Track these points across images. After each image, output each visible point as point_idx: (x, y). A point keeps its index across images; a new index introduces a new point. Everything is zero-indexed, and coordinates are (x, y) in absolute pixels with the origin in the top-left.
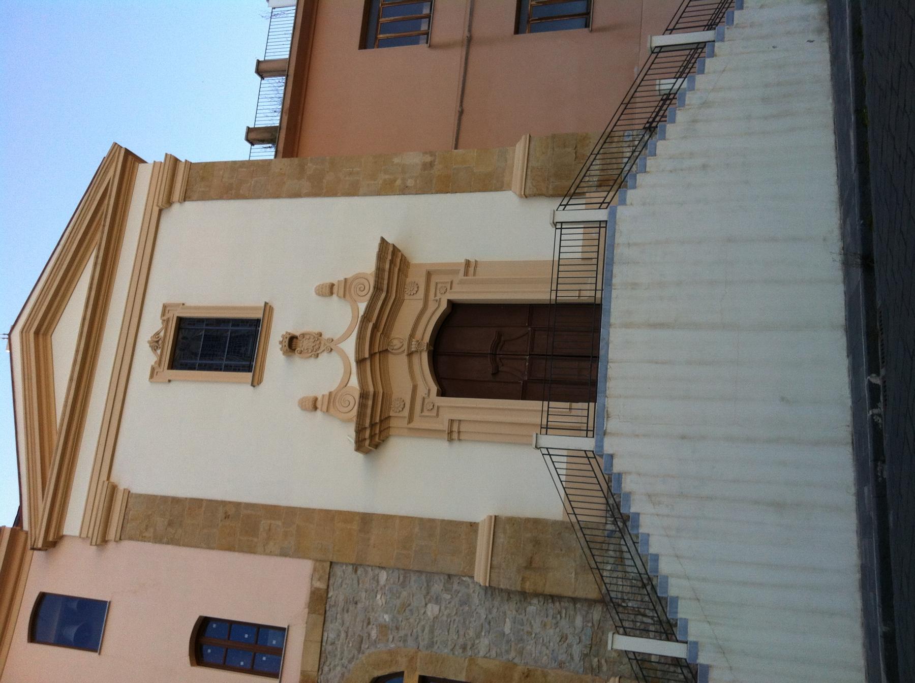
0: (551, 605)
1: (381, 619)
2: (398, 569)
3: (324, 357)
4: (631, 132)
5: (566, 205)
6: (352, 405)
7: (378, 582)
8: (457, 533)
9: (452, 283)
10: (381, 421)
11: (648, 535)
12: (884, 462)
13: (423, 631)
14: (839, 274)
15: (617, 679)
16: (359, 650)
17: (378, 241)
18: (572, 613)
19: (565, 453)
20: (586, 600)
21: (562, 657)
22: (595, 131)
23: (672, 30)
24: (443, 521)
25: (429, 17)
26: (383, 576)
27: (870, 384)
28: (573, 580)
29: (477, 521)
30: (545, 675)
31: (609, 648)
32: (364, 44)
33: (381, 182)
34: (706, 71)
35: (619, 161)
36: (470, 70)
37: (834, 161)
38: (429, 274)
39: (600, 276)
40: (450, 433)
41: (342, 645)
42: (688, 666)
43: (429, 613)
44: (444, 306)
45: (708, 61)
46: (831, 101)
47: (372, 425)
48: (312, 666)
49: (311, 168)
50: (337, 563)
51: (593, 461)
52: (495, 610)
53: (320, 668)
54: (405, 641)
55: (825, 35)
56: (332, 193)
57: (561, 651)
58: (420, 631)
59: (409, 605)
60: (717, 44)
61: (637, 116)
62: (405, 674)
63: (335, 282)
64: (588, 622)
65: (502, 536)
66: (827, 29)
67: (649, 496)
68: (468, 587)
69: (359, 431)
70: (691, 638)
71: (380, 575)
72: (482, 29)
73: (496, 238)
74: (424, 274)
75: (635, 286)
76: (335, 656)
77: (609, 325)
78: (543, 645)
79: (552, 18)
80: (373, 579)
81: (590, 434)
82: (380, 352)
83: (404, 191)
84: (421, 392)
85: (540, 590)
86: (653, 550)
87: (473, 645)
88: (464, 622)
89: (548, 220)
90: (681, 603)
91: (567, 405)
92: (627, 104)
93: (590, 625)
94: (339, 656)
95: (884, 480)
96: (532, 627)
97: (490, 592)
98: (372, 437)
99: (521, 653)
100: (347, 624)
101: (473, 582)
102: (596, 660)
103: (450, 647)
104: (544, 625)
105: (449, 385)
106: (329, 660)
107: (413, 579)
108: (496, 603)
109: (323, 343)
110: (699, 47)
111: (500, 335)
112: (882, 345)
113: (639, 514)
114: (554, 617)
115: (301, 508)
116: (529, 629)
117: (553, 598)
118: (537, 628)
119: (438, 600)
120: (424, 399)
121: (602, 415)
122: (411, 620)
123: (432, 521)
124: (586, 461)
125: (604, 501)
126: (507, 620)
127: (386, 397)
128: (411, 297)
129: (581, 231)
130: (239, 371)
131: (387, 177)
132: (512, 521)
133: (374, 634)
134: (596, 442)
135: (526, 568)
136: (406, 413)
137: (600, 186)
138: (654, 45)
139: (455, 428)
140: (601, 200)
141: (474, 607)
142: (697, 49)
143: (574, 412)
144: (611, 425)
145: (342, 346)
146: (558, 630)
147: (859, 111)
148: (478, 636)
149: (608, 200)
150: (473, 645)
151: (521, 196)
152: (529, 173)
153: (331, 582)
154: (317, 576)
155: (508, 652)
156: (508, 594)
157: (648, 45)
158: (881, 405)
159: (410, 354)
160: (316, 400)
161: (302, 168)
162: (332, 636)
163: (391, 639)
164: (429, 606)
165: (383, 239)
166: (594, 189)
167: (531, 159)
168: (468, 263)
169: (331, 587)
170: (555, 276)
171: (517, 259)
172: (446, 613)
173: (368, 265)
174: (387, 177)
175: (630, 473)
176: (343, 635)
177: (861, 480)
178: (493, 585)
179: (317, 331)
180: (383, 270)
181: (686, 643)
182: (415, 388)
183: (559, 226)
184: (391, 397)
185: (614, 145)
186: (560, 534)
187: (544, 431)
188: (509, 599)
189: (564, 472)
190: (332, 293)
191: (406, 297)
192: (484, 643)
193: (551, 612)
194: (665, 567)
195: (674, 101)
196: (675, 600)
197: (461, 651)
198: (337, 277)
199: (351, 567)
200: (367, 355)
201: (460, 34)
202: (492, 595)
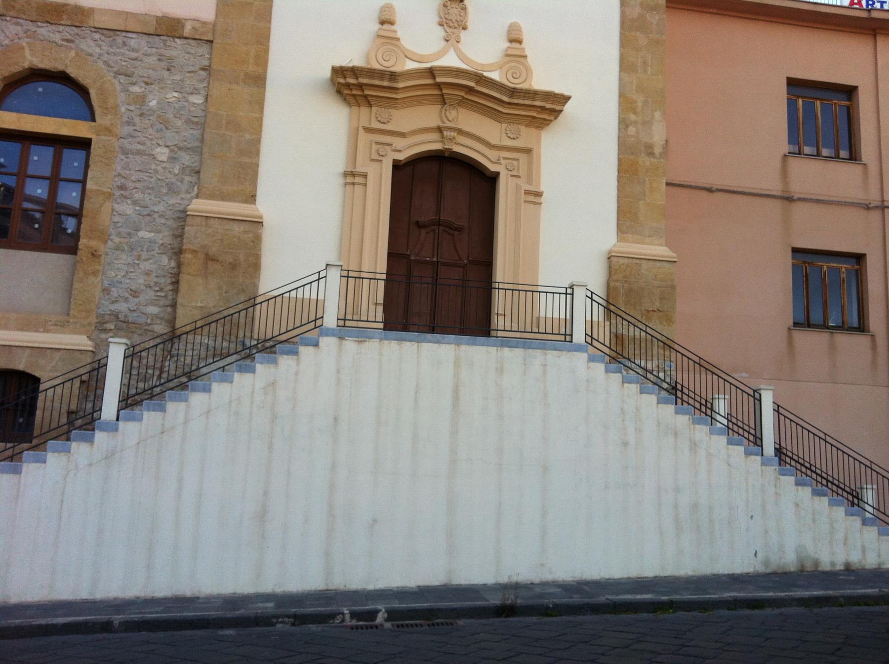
0: (169, 281)
1: (151, 97)
2: (205, 116)
3: (440, 32)
4: (673, 368)
5: (591, 298)
6: (385, 64)
7: (192, 94)
8: (244, 181)
9: (519, 177)
10: (366, 96)
11: (232, 382)
12: (293, 624)
13: (139, 143)
14: (504, 579)
15: (91, 349)
16: (118, 73)
17: (566, 93)
18: (161, 303)
19: (321, 297)
20: (175, 318)
21: (114, 292)
22: (676, 333)
23: (778, 411)
24: (257, 165)
25: (819, 154)
26: (198, 99)
27: (377, 612)
28: (194, 304)
29: (257, 203)
30: (95, 273)
31: (110, 340)
32: (793, 83)
33: (634, 97)
34: (731, 447)
35: (643, 357)
36: (756, 200)
37: (626, 576)
38: (528, 151)
39: (518, 335)
40: (353, 174)
41: (124, 54)
42: (93, 420)
43: (158, 150)
44: (493, 168)
45: (741, 449)
46: (690, 573)
47: (361, 86)
48: (99, 21)
49: (654, 19)
50: (211, 48)
51: (312, 325)
52: (163, 221)
53: (98, 29)
54: (128, 123)
55: (761, 569)
56: (625, 42)
57: (120, 291)
58: (138, 140)
59: (167, 128)
60: (759, 458)
61: (691, 375)
62: (93, 124)
63: (523, 45)
64: (152, 319)
65: (242, 229)
66: (768, 571)
67: (273, 384)
68: (188, 192)
69: (354, 71)
70: (121, 423)
71: (198, 96)
72: (800, 211)
73: (565, 226)
74: (530, 146)
75: (500, 370)
76: (111, 46)
77: (458, 344)
78: (127, 272)
79: (807, 288)
80: (195, 89)
81: (341, 323)
82: (442, 95)
83: (623, 124)
84: (399, 143)
85: (184, 269)
86: (215, 386)
87: (126, 197)
88: (149, 188)
89: (575, 279)
90: (159, 414)
91: (381, 299)
92: (703, 365)
93: (149, 321)
94: (111, 50)
95: (274, 625)
96: (146, 260)
97: (182, 215)
98: (348, 86)
99: (118, 248)
100: (146, 59)
101: (192, 198)
102: (112, 327)
103: (122, 172)
104: (148, 273)
105: (410, 176)
106: (107, 40)
107: (195, 132)
108: (169, 223)
109: (455, 31)
110: (758, 440)
111: (460, 229)
112: (416, 625)
113: (254, 372)
114: (156, 283)
115: (271, 6)
116: (143, 257)
117: (176, 283)
118: (145, 266)
119: (173, 159)
120: (391, 145)
121: (362, 334)
122: (150, 130)
123: (258, 153)
124: (312, 318)
125: (269, 336)
126: (153, 234)
127: (392, 103)
128: (503, 131)
129: (563, 316)
131: (640, 104)
132: (257, 240)
133: (136, 89)
134: (333, 329)
135: (207, 255)
136: (375, 125)
137: (616, 336)
138: (763, 393)
139: (357, 180)
140: (595, 336)
141: (165, 198)
142: (755, 436)
143: (372, 307)
144: (350, 345)
145: (452, 53)
146: (143, 287)
147: (672, 605)
148: (135, 203)
149: (595, 343)
150: (126, 197)
151: (610, 252)
152: (635, 261)
153: (191, 41)
154: (197, 25)
155: (119, 234)
156: (180, 236)
157: (762, 387)
158: (354, 622)
159: (439, 130)
160: (392, 23)
161: (653, 9)
162: (133, 43)
163: (132, 108)
164: (166, 150)
165: (568, 98)
166: (613, 330)
167: (651, 263)
168: (539, 194)
169: (185, 41)
170: (520, 287)
171: (541, 249)
172: (159, 168)
173: (540, 82)
174: (640, 104)
175: (298, 364)
176: (134, 55)
177: (285, 600)
178: (189, 219)
179: (470, 24)
180: (534, 99)
181: (118, 420)
182: (402, 135)
183: (569, 291)
184: (392, 108)
185: (661, 351)
186: (243, 291)
187: (345, 273)
188: (175, 236)
189: (300, 296)
190: (511, 41)
191: (504, 126)
192: (128, 209)
193: (162, 280)
194: (197, 399)
195: (697, 412)
196: (163, 409)
197: (119, 184)
198: (528, 47)
199: (207, 63)
200: (439, 80)
201: (797, 188)
202: (179, 218)
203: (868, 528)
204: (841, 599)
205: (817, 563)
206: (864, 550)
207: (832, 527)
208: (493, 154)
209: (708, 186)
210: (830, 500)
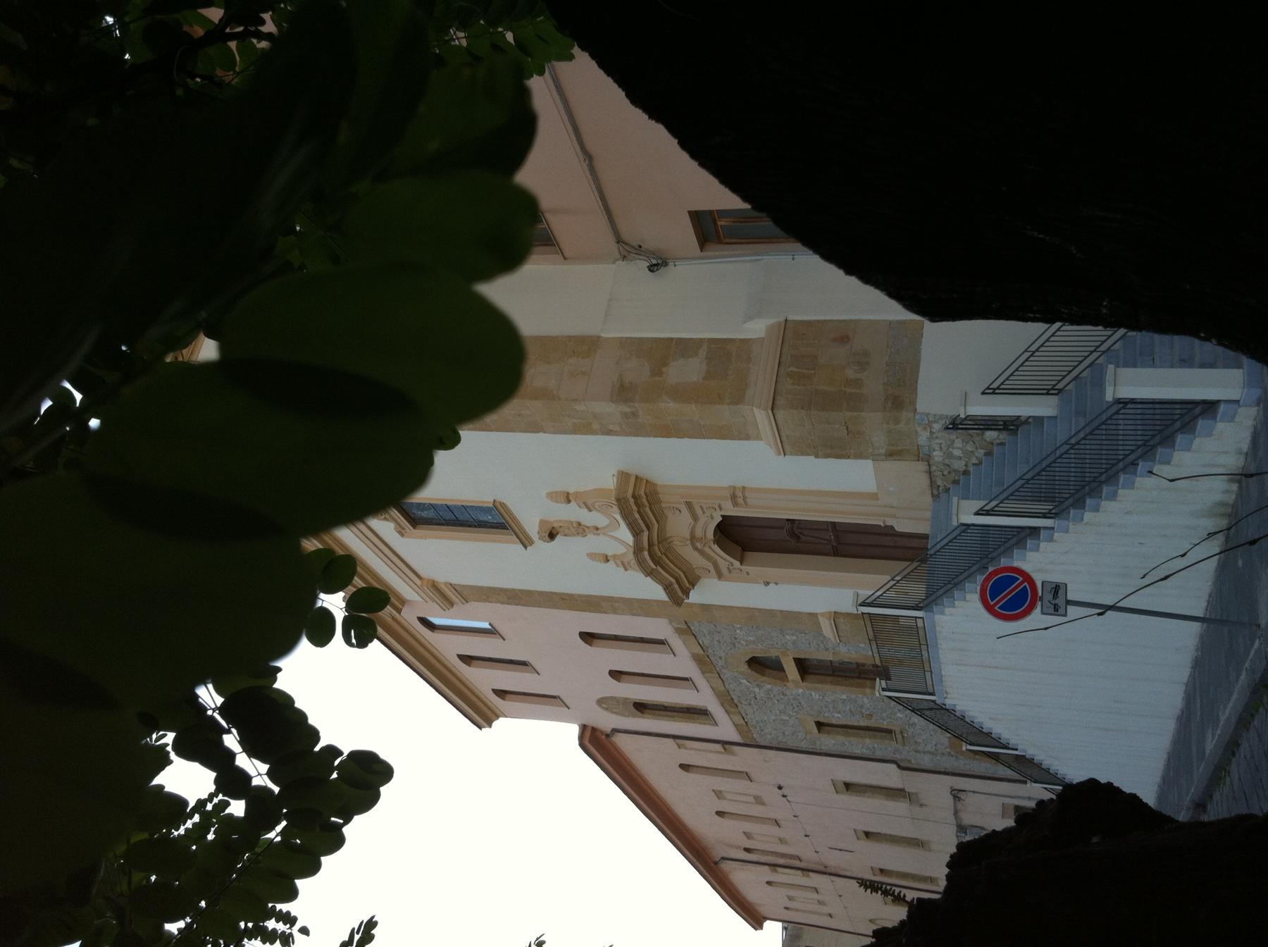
84: (723, 565)
130: (541, 593)
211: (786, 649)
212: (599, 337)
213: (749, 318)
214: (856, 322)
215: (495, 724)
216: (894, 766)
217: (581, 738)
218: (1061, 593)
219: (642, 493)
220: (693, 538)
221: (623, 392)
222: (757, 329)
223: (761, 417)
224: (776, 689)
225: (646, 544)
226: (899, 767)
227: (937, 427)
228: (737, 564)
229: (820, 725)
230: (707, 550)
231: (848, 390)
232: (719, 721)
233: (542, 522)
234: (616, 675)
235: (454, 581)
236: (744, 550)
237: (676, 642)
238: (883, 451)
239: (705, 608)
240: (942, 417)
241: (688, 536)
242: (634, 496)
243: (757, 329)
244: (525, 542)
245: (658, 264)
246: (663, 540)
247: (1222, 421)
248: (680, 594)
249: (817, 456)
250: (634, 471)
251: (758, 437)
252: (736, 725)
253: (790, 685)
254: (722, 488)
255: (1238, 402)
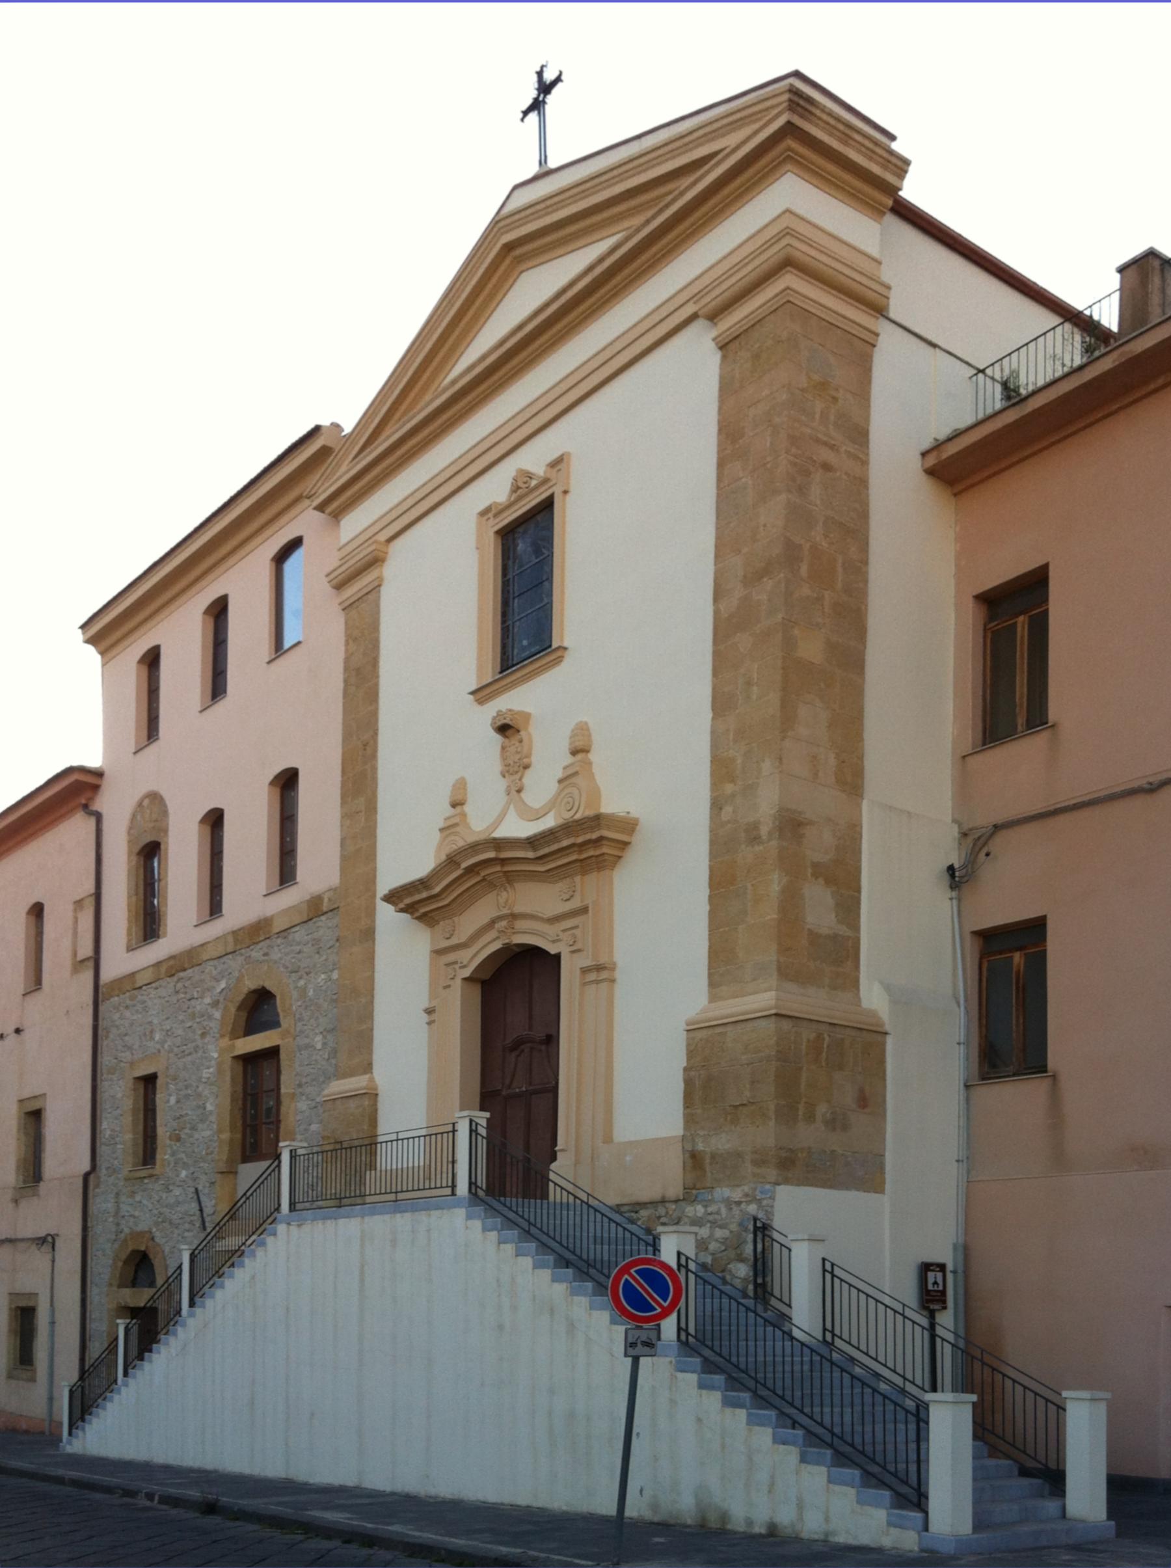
46: (564, 1508)
66: (656, 1519)
84: (464, 955)
120: (456, 963)
130: (374, 716)
167: (743, 1025)
180: (557, 840)
203: (810, 1468)
204: (443, 1552)
205: (724, 1517)
206: (800, 1507)
207: (750, 1459)
208: (552, 930)
209: (1142, 783)
210: (749, 1415)
211: (300, 1037)
212: (861, 797)
213: (888, 988)
214: (884, 1116)
215: (91, 649)
216: (86, 1166)
217: (82, 770)
218: (647, 1350)
219: (605, 850)
220: (514, 916)
221: (791, 825)
222: (873, 998)
223: (762, 999)
224: (214, 1026)
225: (504, 855)
226: (86, 1177)
227: (752, 1209)
228: (467, 973)
229: (149, 1082)
230: (493, 934)
231: (801, 1107)
232: (137, 953)
233: (527, 716)
234: (215, 820)
235: (384, 590)
236: (484, 983)
237: (291, 897)
238: (700, 1146)
239: (369, 934)
240: (769, 1214)
241: (517, 909)
242: (601, 838)
243: (873, 998)
244: (482, 694)
245: (957, 878)
246: (510, 878)
247: (888, 1514)
248: (408, 901)
249: (685, 1069)
250: (636, 839)
251: (713, 998)
252: (133, 974)
253: (225, 1042)
254: (611, 952)
255: (926, 1529)
